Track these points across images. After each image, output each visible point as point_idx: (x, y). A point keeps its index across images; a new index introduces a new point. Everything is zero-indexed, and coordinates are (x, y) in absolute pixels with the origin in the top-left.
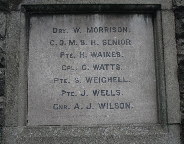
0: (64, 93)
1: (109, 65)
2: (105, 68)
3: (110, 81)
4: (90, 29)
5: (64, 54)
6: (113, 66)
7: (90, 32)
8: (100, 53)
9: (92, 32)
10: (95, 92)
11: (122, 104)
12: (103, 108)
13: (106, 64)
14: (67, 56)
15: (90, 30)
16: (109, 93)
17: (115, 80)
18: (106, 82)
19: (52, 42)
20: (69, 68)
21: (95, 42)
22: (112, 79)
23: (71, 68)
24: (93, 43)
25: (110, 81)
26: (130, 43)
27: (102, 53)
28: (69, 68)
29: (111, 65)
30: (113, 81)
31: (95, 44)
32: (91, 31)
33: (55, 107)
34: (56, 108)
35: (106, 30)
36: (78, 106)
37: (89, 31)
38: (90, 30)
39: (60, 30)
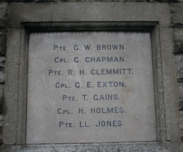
0: (51, 72)
1: (126, 69)
3: (93, 61)
5: (52, 72)
14: (55, 73)
17: (100, 84)
18: (78, 62)
19: (93, 71)
20: (62, 85)
21: (83, 72)
22: (114, 110)
23: (65, 86)
24: (82, 73)
25: (93, 61)
26: (72, 73)
28: (62, 85)
29: (128, 69)
30: (114, 111)
32: (112, 111)
35: (70, 72)
38: (109, 72)
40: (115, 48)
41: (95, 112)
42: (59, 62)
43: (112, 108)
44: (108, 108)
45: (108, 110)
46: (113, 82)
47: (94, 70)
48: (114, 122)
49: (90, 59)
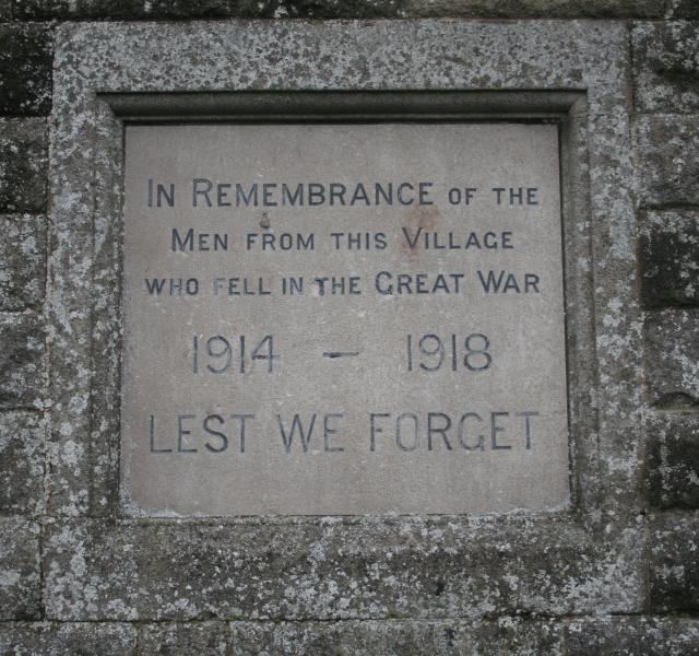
2: (452, 288)
4: (183, 237)
6: (460, 279)
7: (306, 246)
8: (360, 186)
9: (301, 203)
10: (486, 281)
11: (286, 238)
12: (159, 291)
13: (455, 273)
15: (306, 241)
16: (253, 287)
27: (366, 187)
31: (334, 280)
32: (310, 244)
33: (380, 285)
34: (384, 287)
36: (514, 280)
37: (180, 242)
38: (306, 241)
39: (531, 280)
40: (491, 286)
41: (521, 199)
42: (395, 292)
43: (255, 187)
44: (175, 231)
45: (174, 240)
46: (395, 416)
47: (411, 188)
48: (269, 190)
49: (394, 282)
